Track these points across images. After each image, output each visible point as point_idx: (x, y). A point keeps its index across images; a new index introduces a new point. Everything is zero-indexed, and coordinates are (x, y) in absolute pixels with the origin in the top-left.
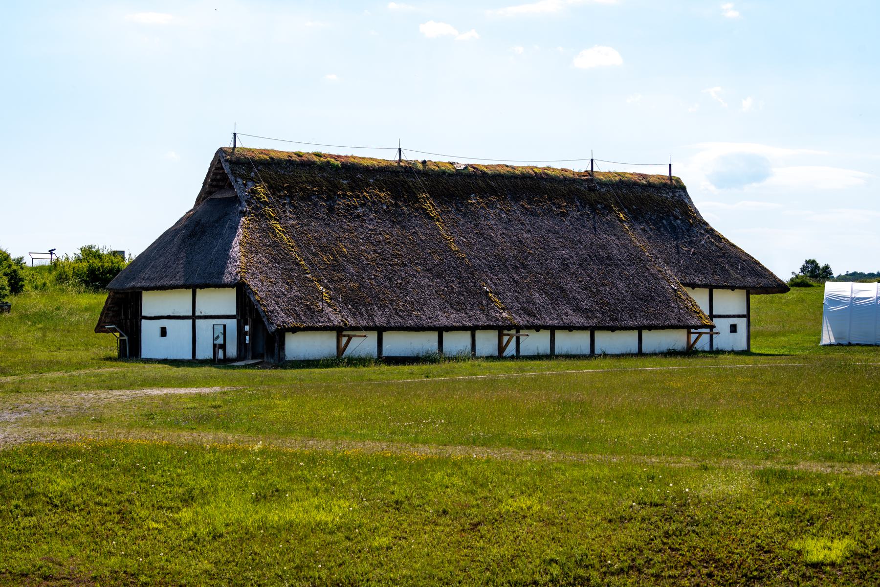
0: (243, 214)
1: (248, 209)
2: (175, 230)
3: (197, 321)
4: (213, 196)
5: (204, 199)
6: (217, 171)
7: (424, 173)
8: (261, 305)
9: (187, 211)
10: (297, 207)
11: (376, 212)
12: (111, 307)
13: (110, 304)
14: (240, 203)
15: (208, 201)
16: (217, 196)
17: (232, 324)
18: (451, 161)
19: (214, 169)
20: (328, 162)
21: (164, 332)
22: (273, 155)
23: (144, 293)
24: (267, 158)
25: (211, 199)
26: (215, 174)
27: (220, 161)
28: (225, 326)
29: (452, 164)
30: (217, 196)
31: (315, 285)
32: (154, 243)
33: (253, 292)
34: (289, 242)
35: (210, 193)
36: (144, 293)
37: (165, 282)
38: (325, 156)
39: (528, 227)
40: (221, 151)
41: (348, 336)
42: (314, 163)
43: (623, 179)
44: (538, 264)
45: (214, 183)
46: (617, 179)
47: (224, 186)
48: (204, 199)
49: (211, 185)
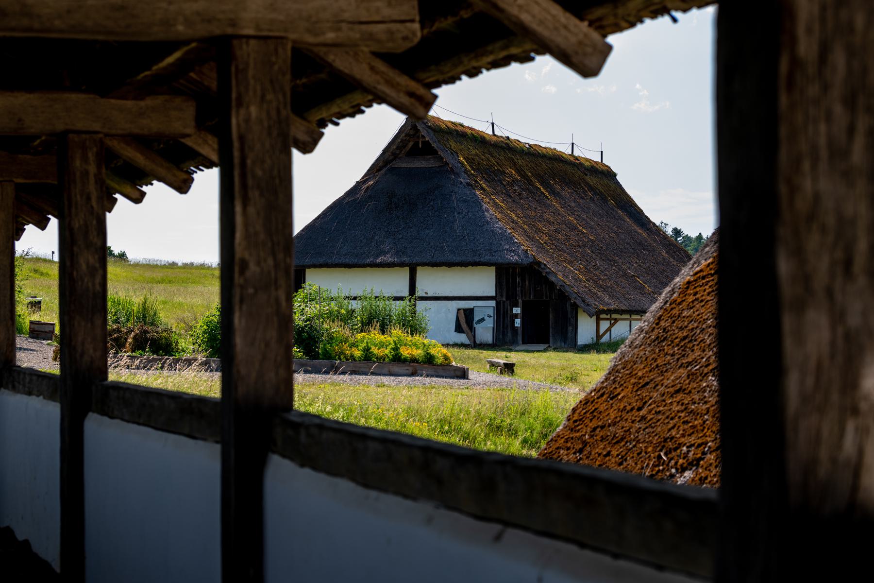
15: (388, 170)
33: (553, 272)
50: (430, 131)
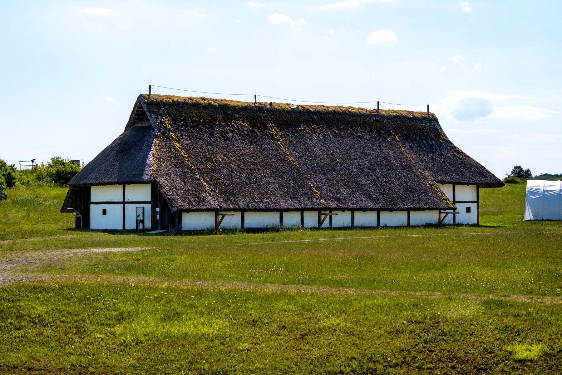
0: (155, 136)
1: (158, 134)
2: (112, 147)
3: (126, 205)
4: (136, 125)
5: (130, 127)
6: (139, 109)
7: (271, 111)
8: (167, 195)
9: (120, 135)
10: (190, 132)
11: (240, 136)
12: (71, 196)
13: (70, 194)
14: (153, 130)
15: (133, 128)
16: (139, 125)
17: (148, 207)
18: (288, 103)
19: (137, 108)
20: (210, 103)
21: (104, 212)
22: (175, 99)
23: (92, 187)
24: (171, 101)
25: (135, 127)
26: (137, 111)
27: (140, 103)
28: (143, 208)
29: (288, 105)
30: (139, 125)
31: (201, 182)
32: (98, 155)
34: (185, 154)
35: (134, 123)
36: (92, 187)
37: (105, 180)
38: (207, 100)
39: (337, 145)
40: (141, 96)
41: (222, 214)
42: (200, 104)
43: (398, 114)
44: (343, 169)
45: (137, 117)
46: (394, 114)
47: (143, 119)
48: (130, 127)
49: (135, 118)
50: (145, 105)
